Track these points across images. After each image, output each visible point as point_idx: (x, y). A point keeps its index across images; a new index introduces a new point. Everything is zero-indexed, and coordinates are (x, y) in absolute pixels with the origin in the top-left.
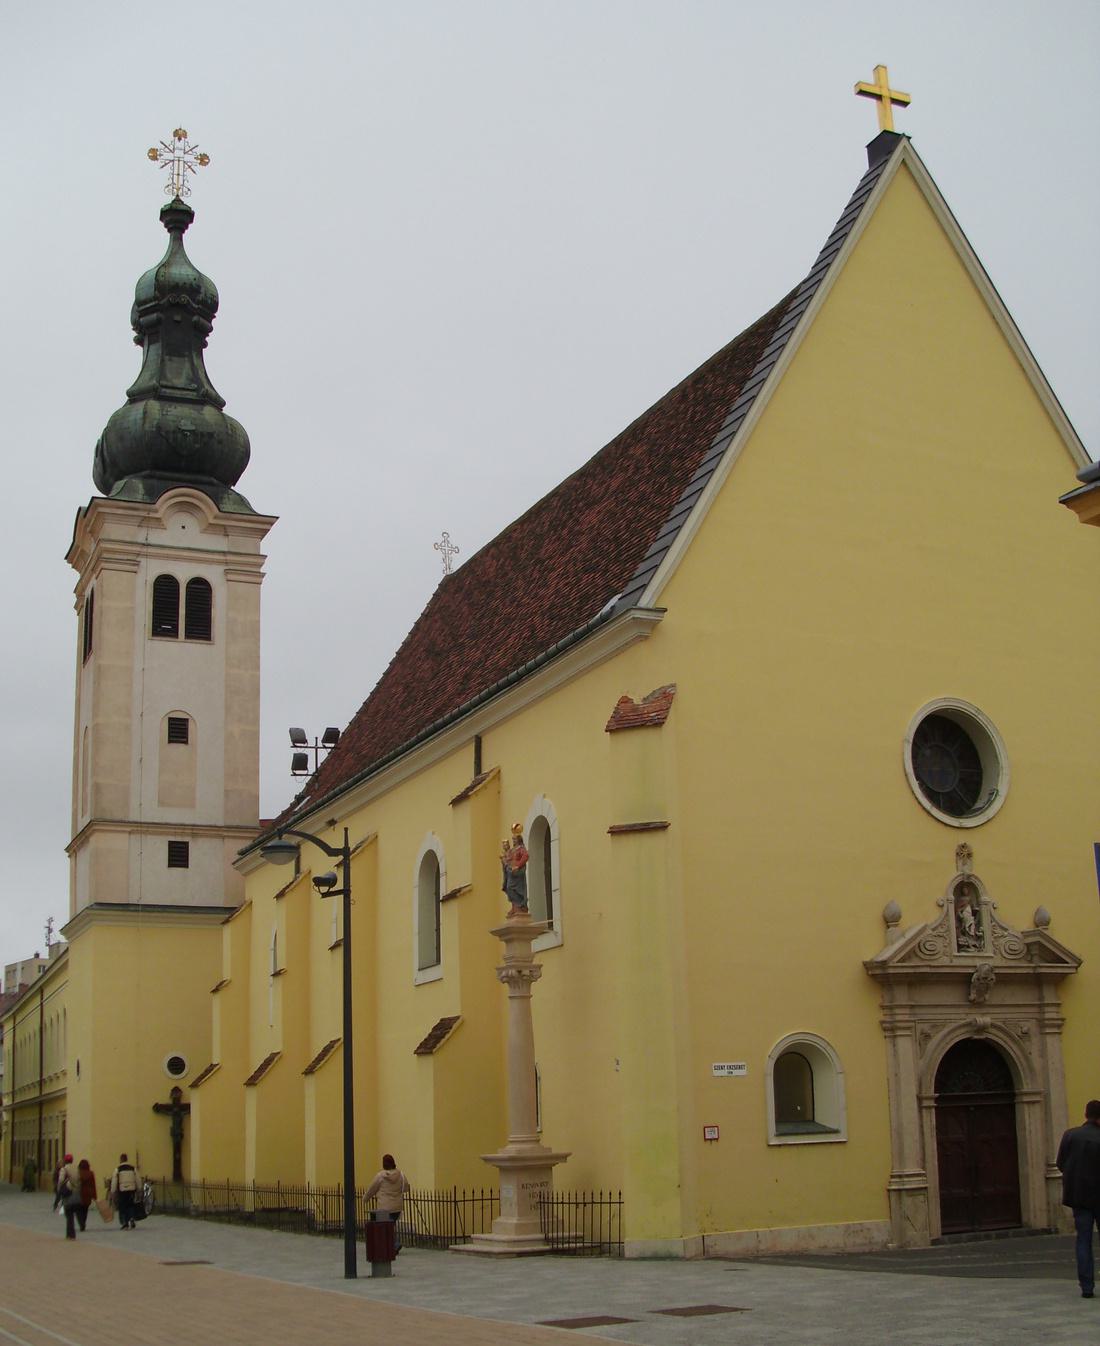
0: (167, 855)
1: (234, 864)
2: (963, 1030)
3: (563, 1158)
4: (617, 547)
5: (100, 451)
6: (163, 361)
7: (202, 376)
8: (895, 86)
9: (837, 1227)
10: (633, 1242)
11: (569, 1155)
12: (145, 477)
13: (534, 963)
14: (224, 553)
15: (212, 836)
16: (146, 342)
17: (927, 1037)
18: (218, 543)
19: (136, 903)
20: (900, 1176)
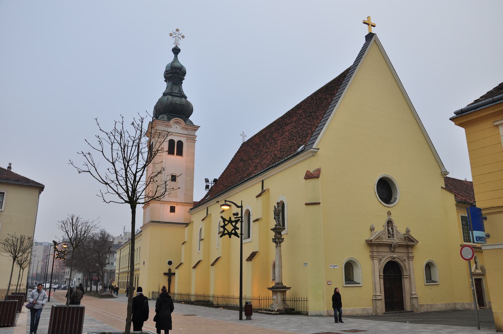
1: (188, 212)
2: (390, 258)
3: (289, 288)
4: (299, 134)
5: (155, 108)
6: (172, 86)
7: (181, 90)
8: (373, 21)
9: (360, 309)
10: (311, 311)
11: (291, 288)
12: (167, 115)
13: (282, 238)
14: (186, 134)
15: (180, 205)
16: (168, 81)
17: (381, 260)
18: (185, 132)
19: (161, 221)
20: (375, 296)
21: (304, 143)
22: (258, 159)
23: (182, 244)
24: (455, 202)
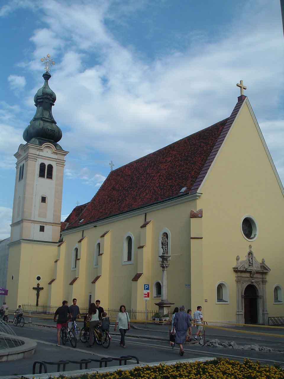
8: (244, 84)
18: (55, 156)
20: (238, 312)
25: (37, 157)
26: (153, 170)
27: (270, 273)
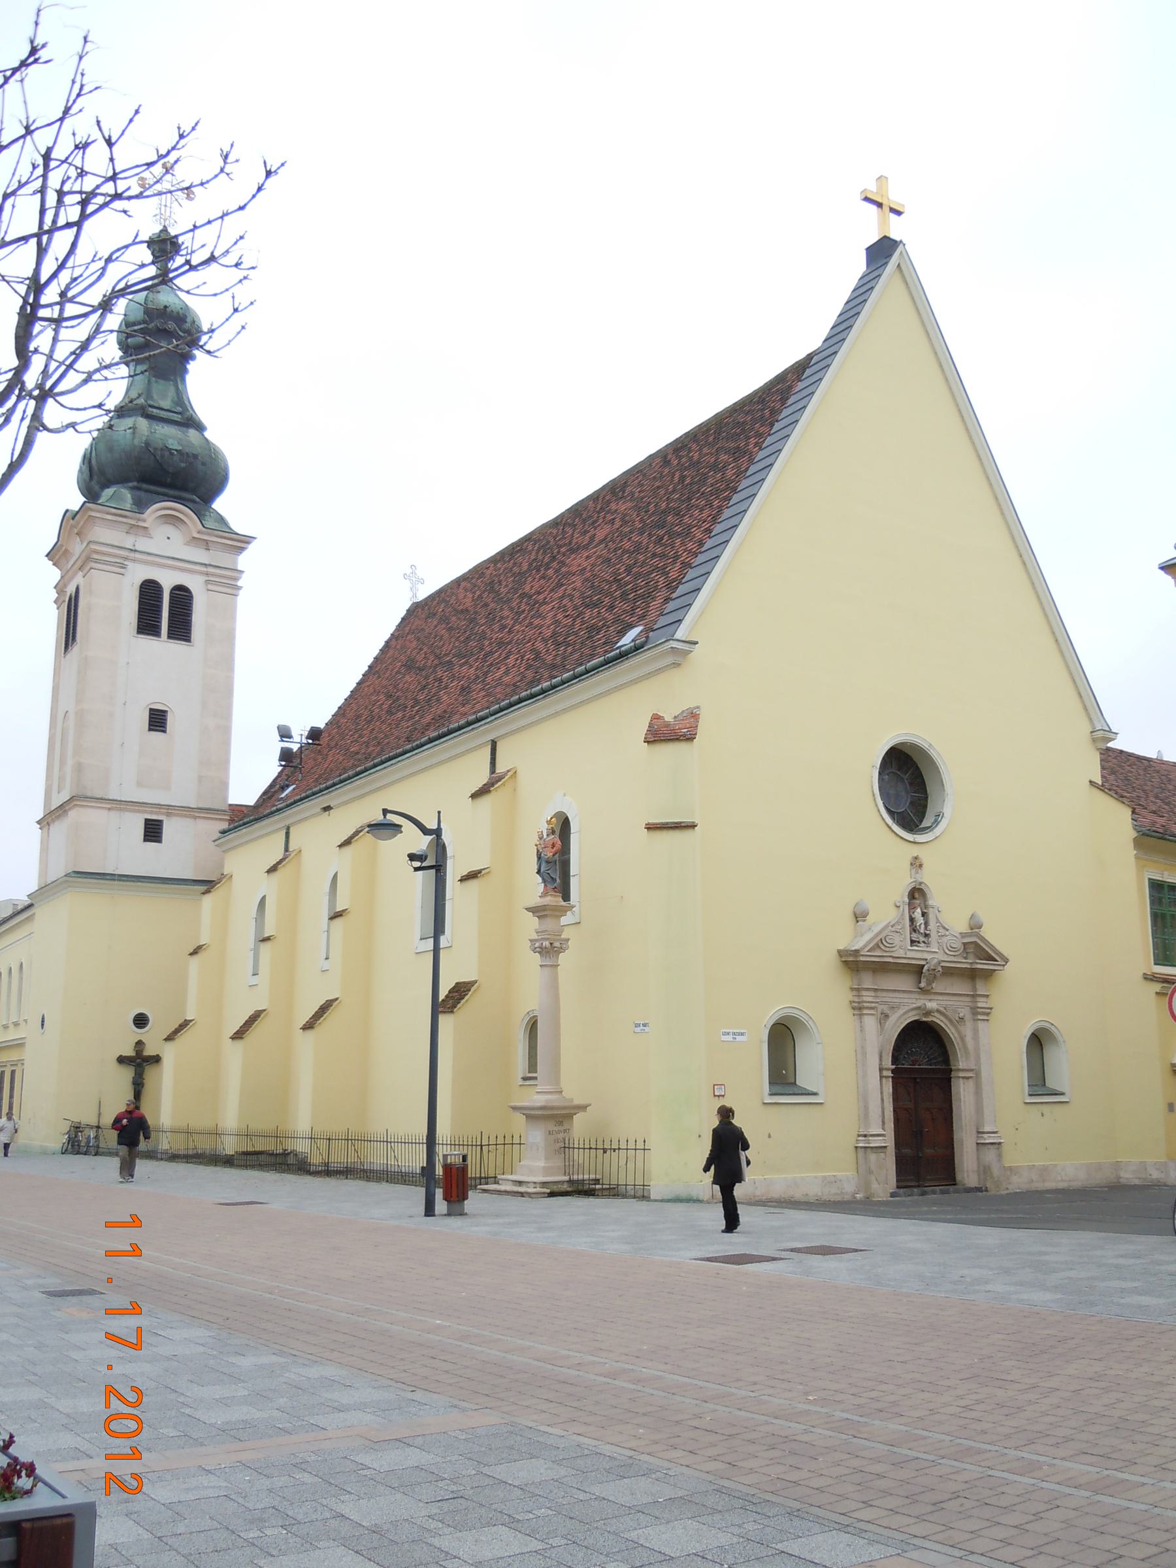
0: (137, 836)
3: (583, 1108)
6: (149, 381)
12: (132, 488)
15: (185, 816)
17: (887, 1016)
20: (865, 1136)
21: (642, 617)
22: (471, 666)
23: (191, 954)
24: (1134, 834)
25: (126, 559)
26: (542, 582)
27: (1009, 975)
